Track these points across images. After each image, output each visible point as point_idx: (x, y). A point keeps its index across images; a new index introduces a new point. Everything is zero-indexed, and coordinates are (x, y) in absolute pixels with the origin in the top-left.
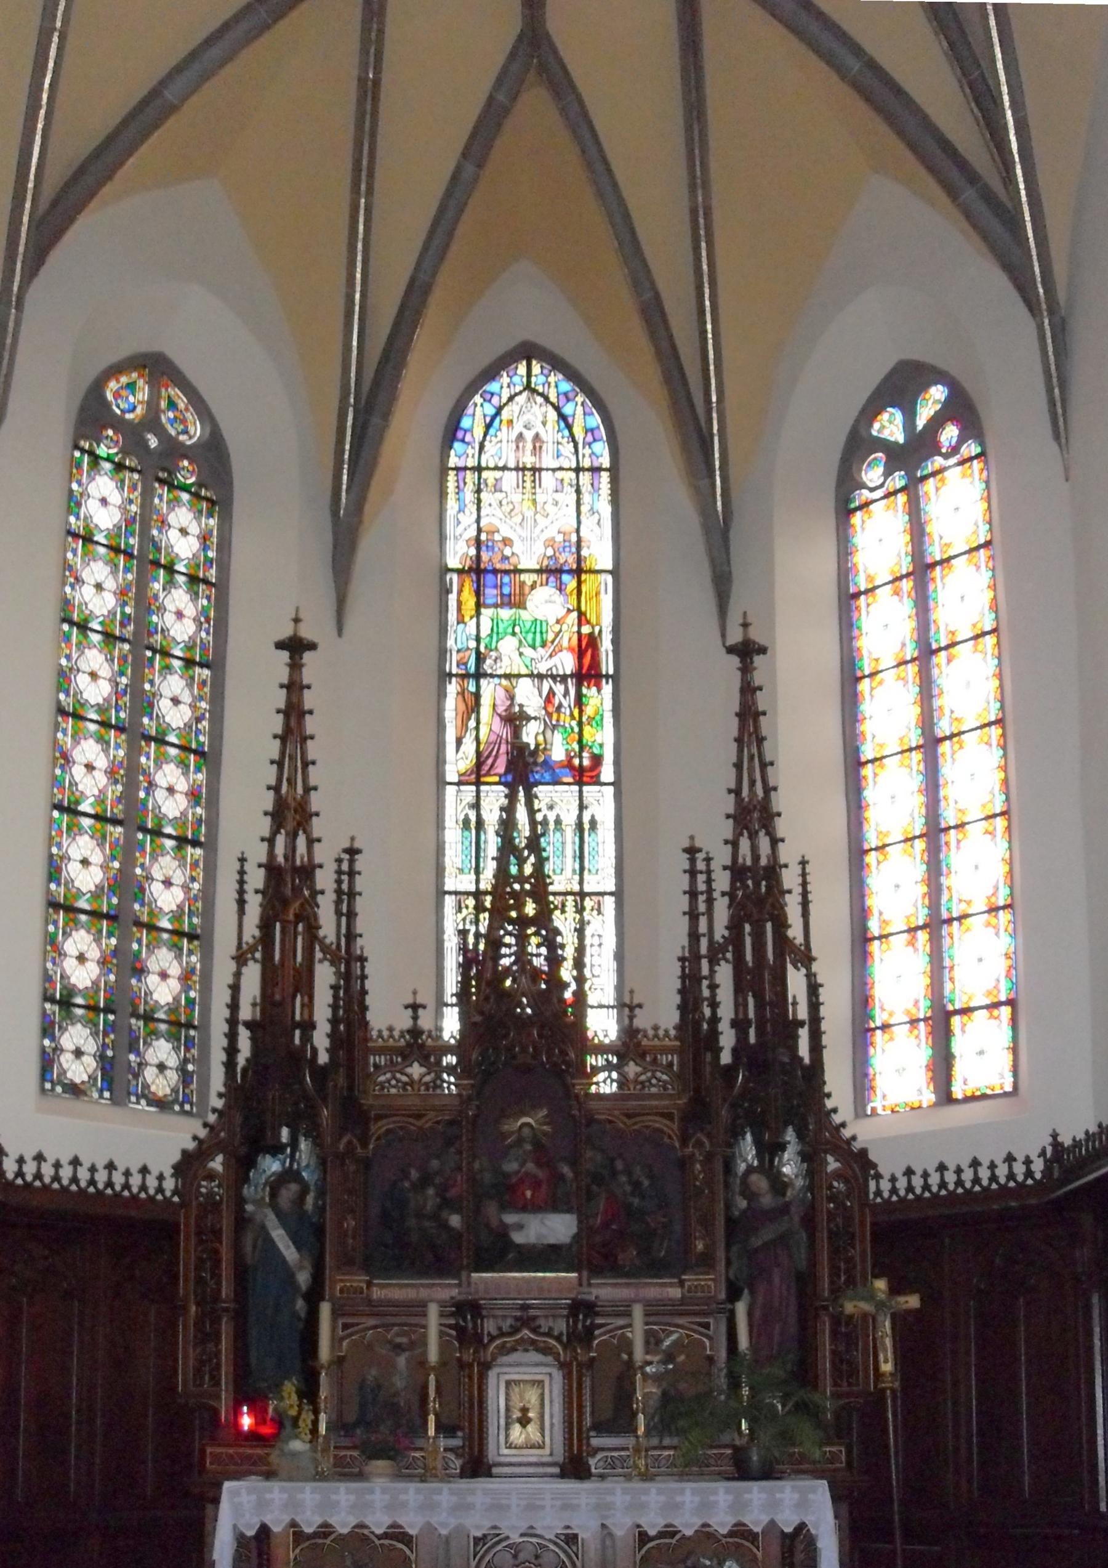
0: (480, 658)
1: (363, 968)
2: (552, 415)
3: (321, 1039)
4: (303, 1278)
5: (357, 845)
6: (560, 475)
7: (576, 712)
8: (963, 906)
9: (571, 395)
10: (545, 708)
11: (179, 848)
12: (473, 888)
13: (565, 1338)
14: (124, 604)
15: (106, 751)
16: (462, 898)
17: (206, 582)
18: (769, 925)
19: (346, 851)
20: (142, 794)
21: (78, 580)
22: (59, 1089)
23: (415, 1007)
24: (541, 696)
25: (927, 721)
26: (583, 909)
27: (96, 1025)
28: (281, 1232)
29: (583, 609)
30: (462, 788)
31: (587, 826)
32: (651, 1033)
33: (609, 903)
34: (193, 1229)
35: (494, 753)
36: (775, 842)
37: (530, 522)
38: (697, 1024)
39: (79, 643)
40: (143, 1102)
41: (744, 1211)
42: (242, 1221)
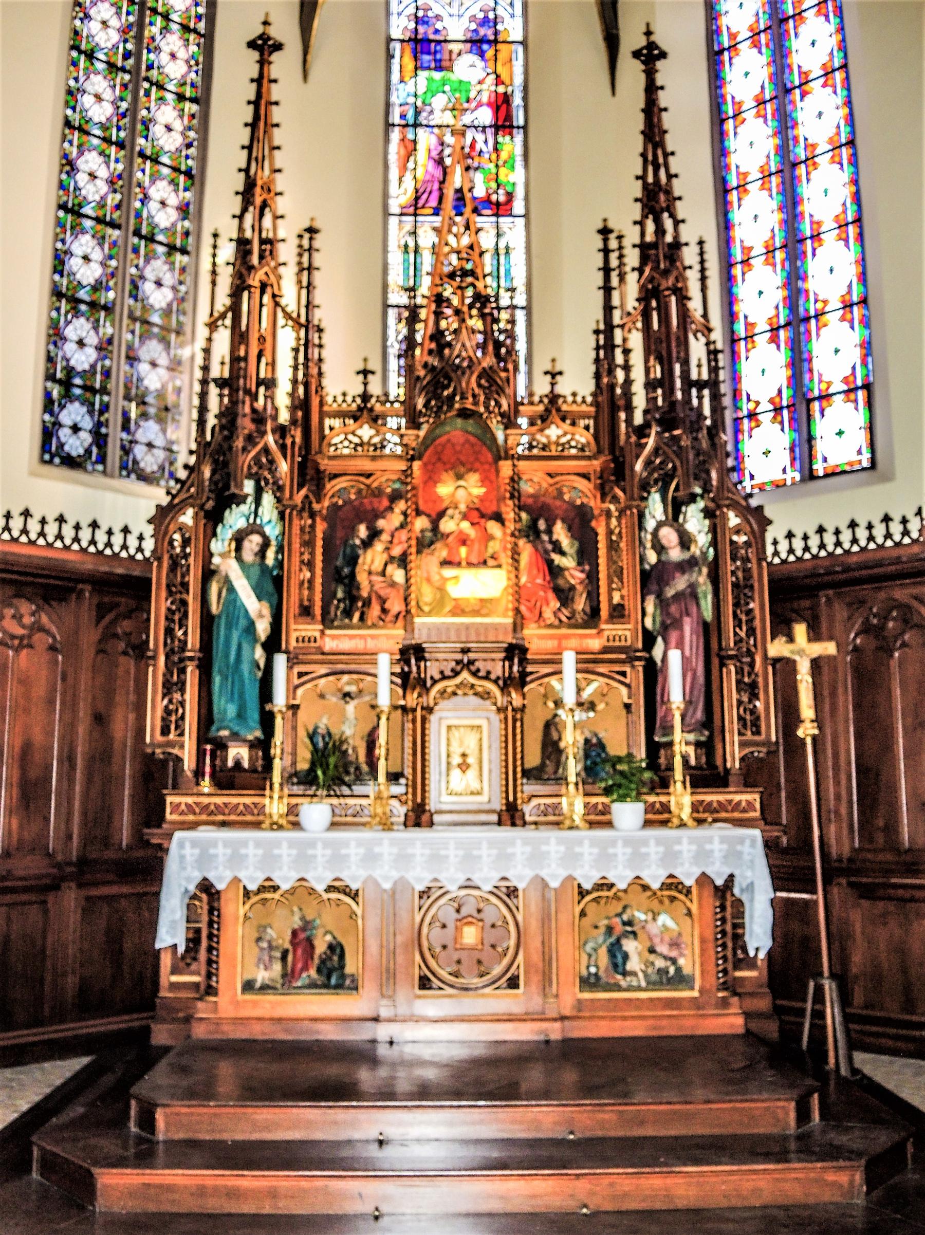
0: (417, 113)
3: (282, 399)
4: (263, 628)
7: (494, 156)
8: (820, 305)
11: (169, 254)
13: (501, 682)
14: (126, 41)
15: (107, 164)
17: (195, 31)
20: (138, 204)
21: (87, 16)
22: (57, 460)
23: (365, 373)
25: (783, 150)
27: (93, 404)
28: (245, 582)
30: (404, 218)
31: (502, 252)
32: (570, 399)
34: (164, 581)
38: (612, 387)
39: (86, 69)
40: (133, 476)
41: (653, 567)
42: (208, 574)
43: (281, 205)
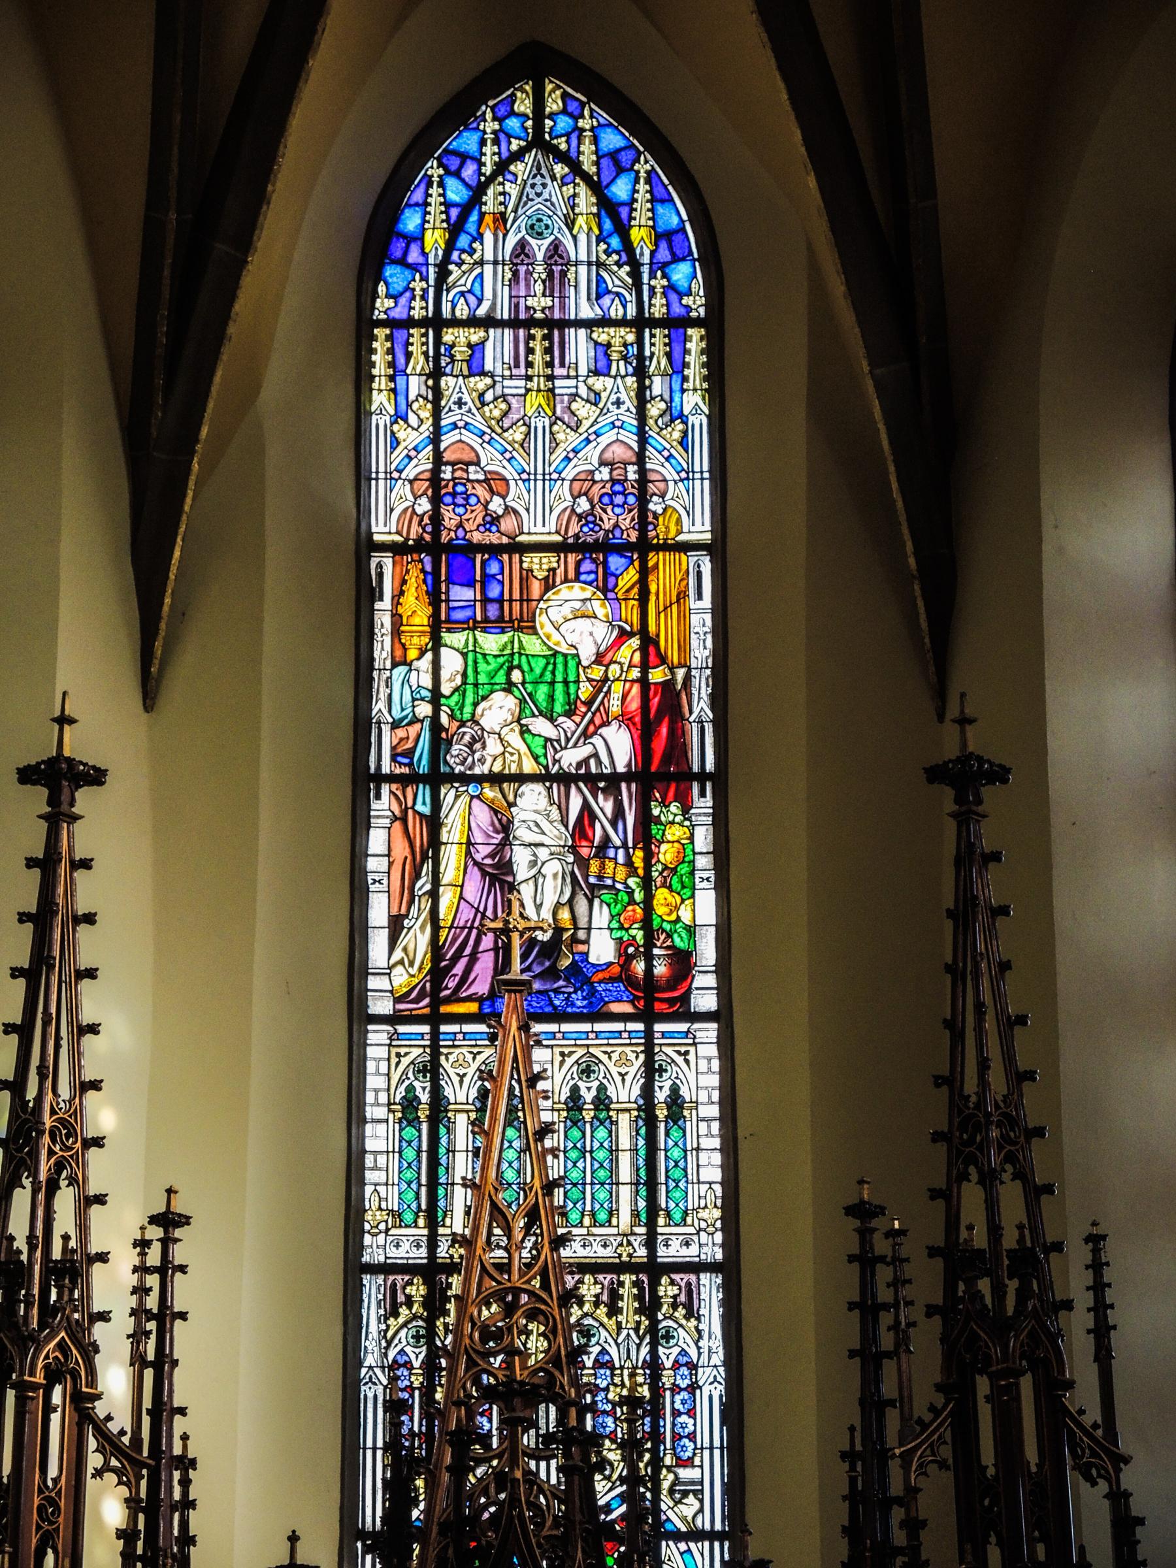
0: (440, 741)
1: (185, 1483)
2: (586, 201)
5: (179, 1206)
6: (601, 335)
7: (638, 857)
9: (626, 158)
10: (574, 849)
12: (420, 1255)
16: (400, 1279)
18: (1026, 1384)
19: (154, 1220)
24: (566, 827)
26: (656, 1303)
29: (652, 628)
31: (661, 1113)
33: (710, 1288)
35: (468, 951)
36: (1036, 1193)
37: (540, 443)
43: (100, 1170)
